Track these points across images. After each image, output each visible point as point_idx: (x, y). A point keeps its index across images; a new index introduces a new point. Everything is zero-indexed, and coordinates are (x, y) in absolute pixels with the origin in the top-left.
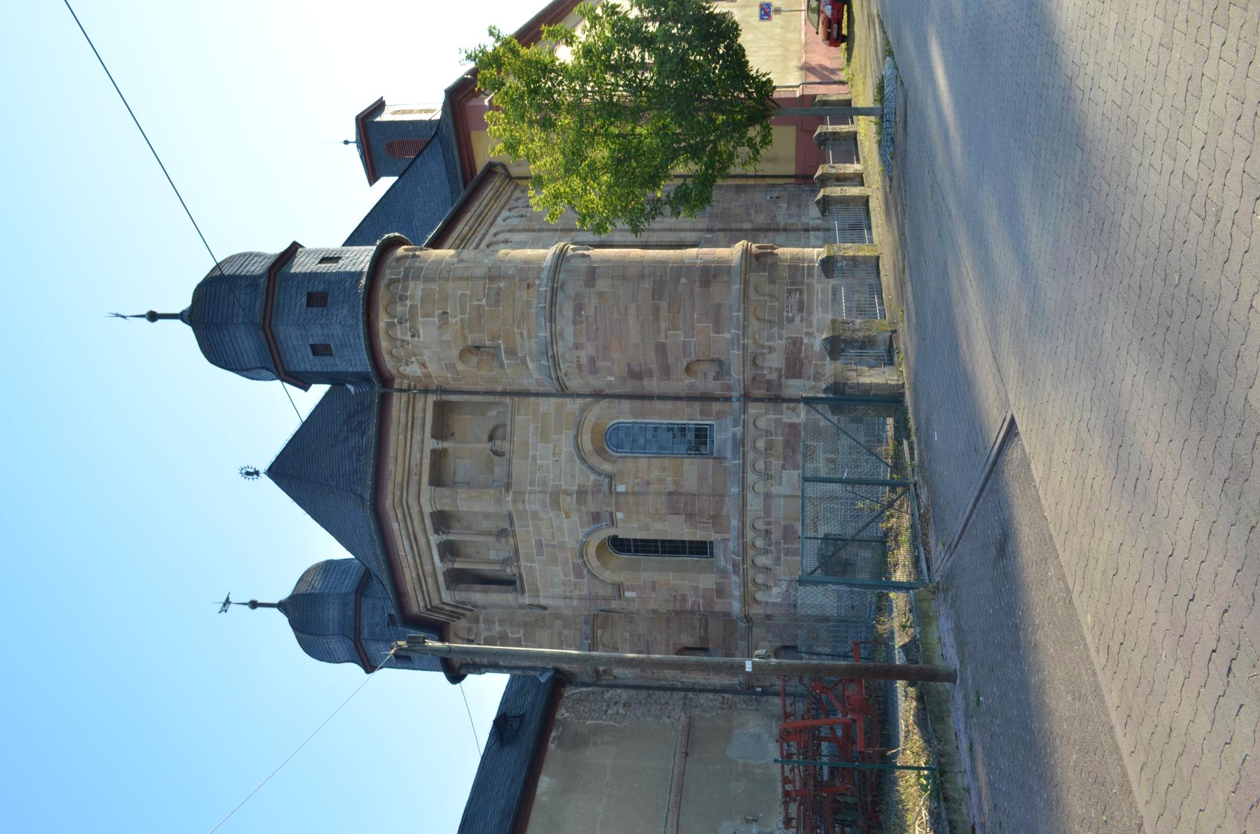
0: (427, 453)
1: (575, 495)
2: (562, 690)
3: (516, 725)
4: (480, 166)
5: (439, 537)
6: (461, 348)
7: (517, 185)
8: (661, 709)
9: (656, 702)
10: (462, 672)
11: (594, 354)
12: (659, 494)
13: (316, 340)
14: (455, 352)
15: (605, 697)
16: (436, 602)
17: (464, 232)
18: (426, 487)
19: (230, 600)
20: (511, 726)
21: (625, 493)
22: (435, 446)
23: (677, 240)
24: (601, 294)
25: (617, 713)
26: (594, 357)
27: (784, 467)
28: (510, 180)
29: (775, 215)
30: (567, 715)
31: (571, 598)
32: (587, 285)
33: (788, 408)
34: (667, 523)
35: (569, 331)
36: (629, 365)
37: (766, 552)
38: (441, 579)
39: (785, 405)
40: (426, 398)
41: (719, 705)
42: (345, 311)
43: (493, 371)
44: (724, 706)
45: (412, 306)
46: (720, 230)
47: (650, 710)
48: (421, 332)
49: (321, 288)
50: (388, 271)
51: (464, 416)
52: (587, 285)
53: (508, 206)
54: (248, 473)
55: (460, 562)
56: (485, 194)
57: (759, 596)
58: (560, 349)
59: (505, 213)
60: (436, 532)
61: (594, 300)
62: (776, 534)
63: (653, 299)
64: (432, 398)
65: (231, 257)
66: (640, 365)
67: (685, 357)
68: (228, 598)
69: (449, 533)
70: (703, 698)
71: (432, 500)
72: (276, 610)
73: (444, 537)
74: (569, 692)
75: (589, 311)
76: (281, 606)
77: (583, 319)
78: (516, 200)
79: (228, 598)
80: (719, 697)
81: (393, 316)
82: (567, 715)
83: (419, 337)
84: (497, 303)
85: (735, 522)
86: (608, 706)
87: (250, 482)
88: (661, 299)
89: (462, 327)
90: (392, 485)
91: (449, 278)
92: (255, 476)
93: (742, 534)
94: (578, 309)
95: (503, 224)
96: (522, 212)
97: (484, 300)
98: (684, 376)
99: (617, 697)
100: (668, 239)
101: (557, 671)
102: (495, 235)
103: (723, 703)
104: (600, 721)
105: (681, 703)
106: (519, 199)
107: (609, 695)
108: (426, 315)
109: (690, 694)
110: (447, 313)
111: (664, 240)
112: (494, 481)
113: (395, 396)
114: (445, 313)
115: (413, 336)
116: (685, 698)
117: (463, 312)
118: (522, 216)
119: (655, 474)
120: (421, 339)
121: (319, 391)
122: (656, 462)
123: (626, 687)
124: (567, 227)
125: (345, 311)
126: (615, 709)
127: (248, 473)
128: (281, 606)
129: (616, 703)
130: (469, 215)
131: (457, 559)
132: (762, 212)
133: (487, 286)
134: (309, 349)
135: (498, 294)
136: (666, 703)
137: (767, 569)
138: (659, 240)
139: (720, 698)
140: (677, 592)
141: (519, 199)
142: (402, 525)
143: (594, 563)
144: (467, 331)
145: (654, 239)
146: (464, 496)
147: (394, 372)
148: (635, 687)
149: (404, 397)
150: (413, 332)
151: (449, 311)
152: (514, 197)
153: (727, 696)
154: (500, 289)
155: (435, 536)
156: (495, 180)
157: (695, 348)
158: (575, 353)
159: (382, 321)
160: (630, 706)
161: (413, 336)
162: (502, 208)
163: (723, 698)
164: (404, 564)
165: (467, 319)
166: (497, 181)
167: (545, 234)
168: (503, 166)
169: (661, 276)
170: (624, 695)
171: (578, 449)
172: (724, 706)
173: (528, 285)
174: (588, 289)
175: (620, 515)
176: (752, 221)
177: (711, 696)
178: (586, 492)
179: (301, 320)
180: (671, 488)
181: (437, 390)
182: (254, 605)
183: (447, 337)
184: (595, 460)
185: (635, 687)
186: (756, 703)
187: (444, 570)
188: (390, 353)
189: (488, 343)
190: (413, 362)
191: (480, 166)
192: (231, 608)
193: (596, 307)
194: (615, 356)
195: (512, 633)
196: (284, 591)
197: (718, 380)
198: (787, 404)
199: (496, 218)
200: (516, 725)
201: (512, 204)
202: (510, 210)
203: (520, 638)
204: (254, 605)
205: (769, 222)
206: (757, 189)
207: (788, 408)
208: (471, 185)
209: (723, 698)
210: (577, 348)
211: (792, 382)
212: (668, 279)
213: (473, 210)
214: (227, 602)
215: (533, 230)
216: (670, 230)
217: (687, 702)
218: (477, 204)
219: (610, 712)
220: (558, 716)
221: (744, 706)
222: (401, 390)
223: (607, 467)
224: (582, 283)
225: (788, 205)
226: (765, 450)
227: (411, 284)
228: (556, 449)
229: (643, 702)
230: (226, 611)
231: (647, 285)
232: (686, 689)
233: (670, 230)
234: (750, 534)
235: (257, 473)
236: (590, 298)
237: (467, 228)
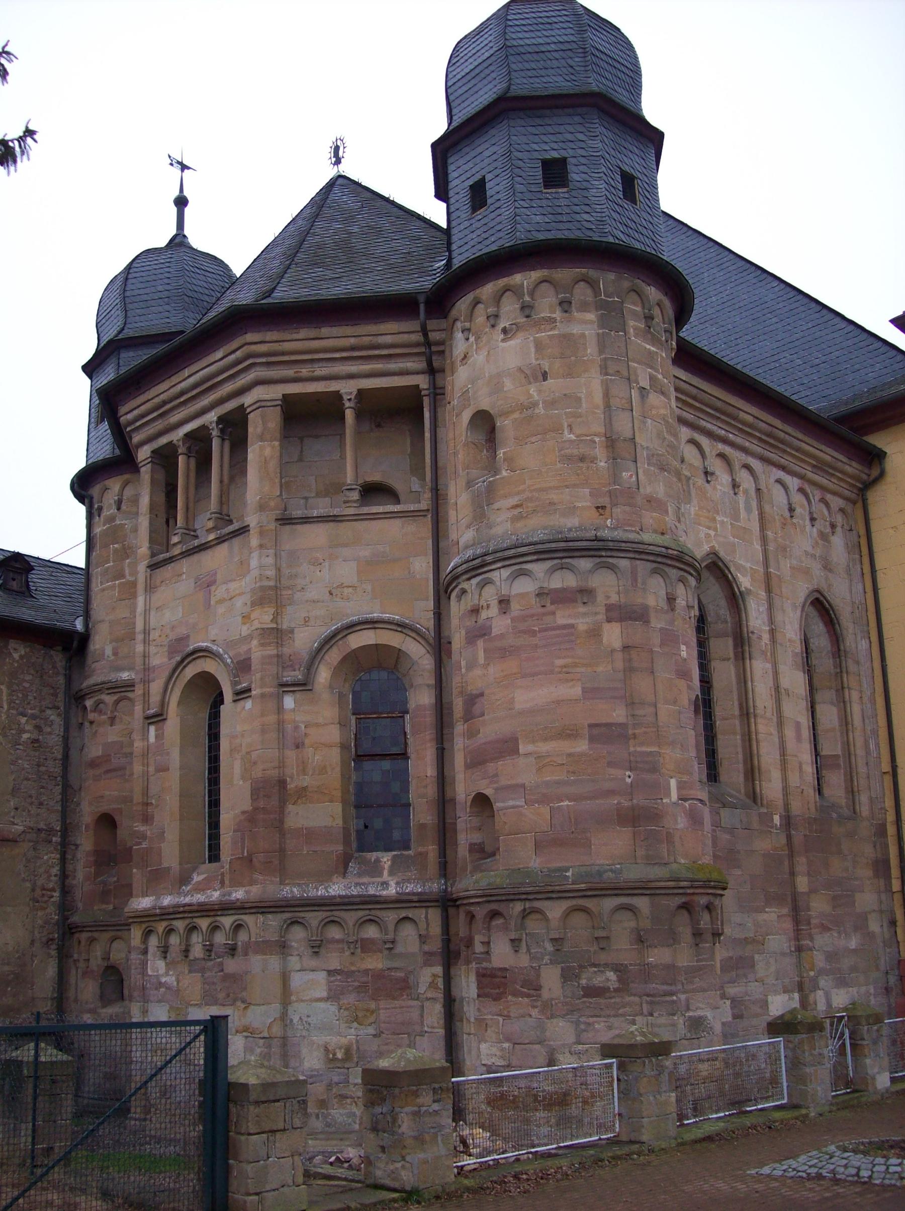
0: (333, 386)
1: (274, 626)
2: (60, 648)
3: (14, 585)
4: (877, 440)
5: (214, 425)
6: (491, 412)
7: (854, 503)
8: (31, 796)
9: (43, 787)
10: (86, 501)
11: (495, 631)
12: (282, 765)
13: (491, 188)
14: (485, 404)
15: (49, 712)
16: (136, 438)
17: (742, 415)
18: (276, 392)
19: (186, 171)
20: (14, 580)
21: (280, 709)
22: (346, 397)
23: (763, 765)
24: (595, 633)
25: (22, 731)
26: (490, 633)
27: (330, 973)
28: (860, 490)
29: (829, 929)
30: (16, 656)
31: (146, 642)
32: (609, 608)
33: (435, 976)
34: (241, 783)
35: (525, 586)
36: (482, 695)
37: (209, 949)
38: (163, 440)
39: (439, 970)
40: (423, 373)
41: (40, 883)
42: (538, 219)
43: (463, 470)
44: (38, 892)
45: (554, 320)
46: (789, 837)
47: (27, 779)
48: (512, 343)
49: (574, 176)
50: (611, 276)
51: (408, 441)
52: (609, 608)
53: (807, 487)
54: (337, 149)
55: (188, 464)
56: (823, 447)
57: (153, 941)
58: (496, 573)
59: (793, 483)
60: (221, 420)
61: (582, 625)
62: (232, 965)
63: (591, 726)
64: (422, 381)
65: (618, 29)
66: (483, 715)
67: (496, 789)
68: (188, 168)
69: (223, 440)
70: (50, 857)
71: (260, 404)
72: (173, 231)
73: (215, 433)
74: (58, 658)
75: (562, 617)
76: (179, 241)
77: (549, 607)
78: (823, 500)
79: (188, 168)
80: (53, 883)
81: (532, 293)
82: (16, 656)
83: (503, 340)
84: (569, 459)
85: (239, 894)
86: (33, 717)
87: (326, 153)
88: (592, 739)
89: (522, 408)
90: (275, 338)
91: (607, 374)
92: (334, 160)
93: (226, 908)
94: (563, 597)
95: (772, 480)
96: (799, 510)
97: (572, 437)
98: (474, 790)
99: (49, 730)
100: (763, 751)
101: (84, 639)
102: (747, 467)
103: (44, 889)
104: (6, 707)
105: (42, 825)
106: (827, 504)
107: (52, 717)
108: (539, 346)
109: (56, 839)
110: (545, 379)
111: (762, 744)
112: (306, 498)
113: (415, 325)
114: (545, 376)
115: (505, 331)
116: (50, 831)
117: (551, 404)
118: (791, 510)
119: (315, 758)
120: (501, 344)
121: (437, 212)
122: (335, 756)
123: (66, 740)
124: (774, 582)
125: (538, 219)
126: (28, 728)
127: (337, 149)
128: (179, 241)
129: (38, 728)
130: (777, 423)
131: (193, 462)
132: (834, 907)
133: (597, 439)
134: (478, 177)
135: (582, 459)
136: (41, 804)
137: (186, 952)
138: (761, 737)
139: (51, 885)
140: (157, 806)
141: (827, 504)
142: (221, 363)
143: (190, 672)
144: (516, 415)
145: (761, 728)
146: (268, 452)
147: (454, 313)
148: (66, 757)
149: (417, 337)
150: (511, 330)
151: (550, 381)
152: (829, 497)
153: (57, 894)
154: (593, 460)
155: (215, 418)
156: (854, 464)
157: (513, 807)
158: (494, 604)
159: (523, 279)
160: (35, 749)
161: (505, 331)
162: (802, 477)
163: (53, 890)
164: (175, 379)
165: (537, 411)
166: (852, 468)
167: (758, 547)
168: (882, 474)
169: (635, 736)
170: (54, 739)
171: (351, 628)
172: (38, 892)
173: (603, 508)
174: (602, 609)
175: (248, 704)
176: (813, 891)
177: (55, 870)
178: (279, 644)
179: (519, 155)
180: (291, 786)
181: (435, 388)
182: (181, 202)
183: (508, 384)
184: (334, 656)
185: (66, 757)
186: (44, 939)
187: (175, 442)
188: (477, 302)
189: (501, 453)
190: (467, 339)
191: (877, 440)
192: (176, 171)
193: (572, 626)
194: (491, 670)
195: (129, 563)
196: (198, 239)
197: (470, 851)
198: (441, 974)
199: (783, 468)
200: (14, 585)
201: (816, 494)
202: (801, 490)
203: (123, 576)
204: (181, 202)
205: (814, 921)
206: (883, 897)
207: (435, 976)
208: (844, 430)
209: (53, 890)
210: (500, 602)
211: (473, 978)
212: (632, 749)
213: (789, 429)
214: (184, 167)
215: (763, 528)
216: (783, 753)
217: (43, 835)
218: (800, 435)
219: (23, 720)
220: (12, 644)
221: (40, 922)
222: (425, 332)
223: (323, 675)
224: (614, 599)
225: (855, 951)
226: (362, 940)
227: (591, 316)
228: (350, 590)
229: (43, 769)
230: (172, 164)
231: (619, 714)
232: (66, 830)
233: (783, 753)
234: (227, 921)
235: (338, 161)
236: (585, 615)
237: (749, 419)
